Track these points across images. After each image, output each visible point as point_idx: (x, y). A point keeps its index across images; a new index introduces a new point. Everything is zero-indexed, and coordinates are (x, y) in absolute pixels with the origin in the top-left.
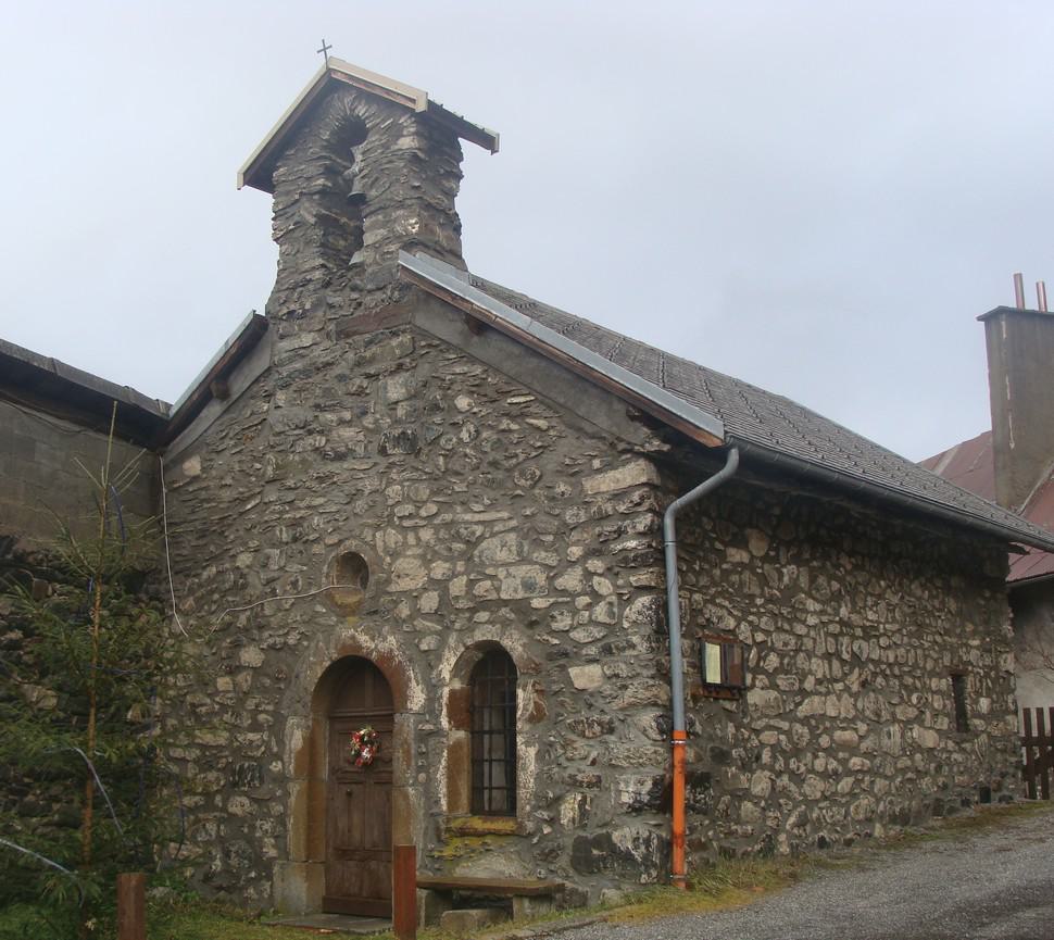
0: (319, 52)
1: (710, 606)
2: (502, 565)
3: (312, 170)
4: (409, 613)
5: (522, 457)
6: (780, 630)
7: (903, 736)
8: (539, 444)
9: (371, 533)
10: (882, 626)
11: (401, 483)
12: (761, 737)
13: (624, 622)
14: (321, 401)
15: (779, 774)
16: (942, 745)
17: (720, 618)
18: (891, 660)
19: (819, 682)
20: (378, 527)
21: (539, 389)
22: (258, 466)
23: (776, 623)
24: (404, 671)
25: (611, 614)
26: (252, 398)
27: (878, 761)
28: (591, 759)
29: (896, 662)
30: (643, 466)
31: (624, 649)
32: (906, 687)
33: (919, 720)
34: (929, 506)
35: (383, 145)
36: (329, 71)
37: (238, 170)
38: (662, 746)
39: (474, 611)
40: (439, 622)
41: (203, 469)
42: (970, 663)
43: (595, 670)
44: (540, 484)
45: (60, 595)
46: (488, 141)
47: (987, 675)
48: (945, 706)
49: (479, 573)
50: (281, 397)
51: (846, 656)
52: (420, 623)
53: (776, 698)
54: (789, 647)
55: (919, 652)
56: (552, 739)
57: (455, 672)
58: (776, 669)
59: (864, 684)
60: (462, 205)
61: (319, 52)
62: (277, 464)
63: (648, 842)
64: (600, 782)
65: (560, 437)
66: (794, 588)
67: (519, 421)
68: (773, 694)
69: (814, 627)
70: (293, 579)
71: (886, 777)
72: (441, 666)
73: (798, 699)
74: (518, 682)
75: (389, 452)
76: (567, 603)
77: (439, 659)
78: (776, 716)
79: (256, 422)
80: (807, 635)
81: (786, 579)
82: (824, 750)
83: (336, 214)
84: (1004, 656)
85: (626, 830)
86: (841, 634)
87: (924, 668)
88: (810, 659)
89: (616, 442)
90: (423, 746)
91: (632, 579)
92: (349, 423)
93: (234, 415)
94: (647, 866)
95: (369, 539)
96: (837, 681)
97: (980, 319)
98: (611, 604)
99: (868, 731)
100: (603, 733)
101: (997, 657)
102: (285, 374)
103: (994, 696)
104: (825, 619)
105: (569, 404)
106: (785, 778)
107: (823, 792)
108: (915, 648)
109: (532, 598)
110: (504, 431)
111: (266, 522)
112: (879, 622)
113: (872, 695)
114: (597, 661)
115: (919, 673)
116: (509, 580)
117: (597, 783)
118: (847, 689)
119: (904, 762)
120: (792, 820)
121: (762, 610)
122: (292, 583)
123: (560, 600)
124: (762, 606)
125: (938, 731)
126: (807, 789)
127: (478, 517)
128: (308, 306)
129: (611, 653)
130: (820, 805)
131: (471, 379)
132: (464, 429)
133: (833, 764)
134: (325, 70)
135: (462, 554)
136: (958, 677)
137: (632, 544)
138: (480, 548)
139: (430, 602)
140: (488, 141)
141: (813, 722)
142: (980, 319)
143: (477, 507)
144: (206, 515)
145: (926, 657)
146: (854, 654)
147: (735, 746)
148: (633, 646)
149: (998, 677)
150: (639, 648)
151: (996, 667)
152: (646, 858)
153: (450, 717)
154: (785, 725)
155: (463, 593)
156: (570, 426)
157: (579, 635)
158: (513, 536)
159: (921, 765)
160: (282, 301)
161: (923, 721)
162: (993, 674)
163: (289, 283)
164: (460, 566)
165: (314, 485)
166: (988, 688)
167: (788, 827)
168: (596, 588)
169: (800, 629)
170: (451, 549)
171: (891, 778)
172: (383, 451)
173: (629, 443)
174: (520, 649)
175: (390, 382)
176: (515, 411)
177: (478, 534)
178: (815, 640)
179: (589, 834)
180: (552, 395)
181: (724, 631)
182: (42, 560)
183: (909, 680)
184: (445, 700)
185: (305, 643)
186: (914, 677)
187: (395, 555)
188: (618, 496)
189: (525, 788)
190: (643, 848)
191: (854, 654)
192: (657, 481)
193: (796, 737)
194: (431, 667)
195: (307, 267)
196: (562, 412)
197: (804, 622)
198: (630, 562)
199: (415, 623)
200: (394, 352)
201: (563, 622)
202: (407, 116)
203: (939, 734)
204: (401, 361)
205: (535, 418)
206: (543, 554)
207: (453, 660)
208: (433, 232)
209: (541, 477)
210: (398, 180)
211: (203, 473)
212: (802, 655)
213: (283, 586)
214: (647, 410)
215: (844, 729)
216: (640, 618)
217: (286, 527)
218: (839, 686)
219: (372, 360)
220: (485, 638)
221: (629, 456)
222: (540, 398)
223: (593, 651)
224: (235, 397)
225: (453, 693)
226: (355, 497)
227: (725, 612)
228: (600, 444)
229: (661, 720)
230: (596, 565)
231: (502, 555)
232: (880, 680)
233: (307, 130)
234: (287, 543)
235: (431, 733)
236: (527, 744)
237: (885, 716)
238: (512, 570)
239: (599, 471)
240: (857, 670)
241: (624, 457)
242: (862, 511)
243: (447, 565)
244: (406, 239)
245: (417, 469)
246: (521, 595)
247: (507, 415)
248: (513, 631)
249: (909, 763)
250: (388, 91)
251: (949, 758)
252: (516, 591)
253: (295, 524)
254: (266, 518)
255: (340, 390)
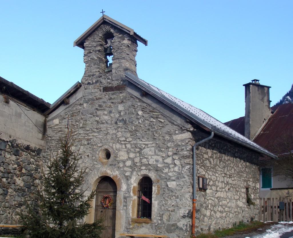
0: (101, 12)
1: (200, 169)
2: (150, 155)
3: (95, 44)
4: (122, 166)
5: (156, 128)
6: (213, 175)
7: (236, 203)
8: (161, 126)
9: (112, 144)
10: (233, 175)
11: (121, 132)
12: (209, 202)
13: (183, 172)
14: (98, 108)
15: (212, 211)
16: (244, 206)
17: (202, 172)
18: (234, 184)
19: (220, 188)
20: (114, 143)
21: (162, 112)
22: (77, 123)
23: (212, 173)
24: (121, 180)
25: (179, 170)
26: (76, 104)
27: (230, 209)
28: (172, 205)
29: (235, 184)
30: (189, 135)
31: (182, 178)
32: (237, 191)
33: (239, 199)
34: (251, 147)
35: (119, 42)
36: (103, 18)
37: (74, 40)
38: (191, 202)
39: (141, 166)
40: (131, 168)
41: (60, 123)
42: (250, 185)
43: (174, 183)
44: (161, 136)
45: (25, 155)
46: (145, 42)
47: (253, 189)
48: (244, 196)
49: (143, 157)
50: (85, 105)
51: (226, 182)
52: (125, 169)
53: (212, 192)
54: (215, 179)
55: (240, 182)
56: (162, 199)
57: (135, 182)
58: (212, 185)
59: (229, 189)
60: (137, 58)
61: (101, 12)
62: (83, 123)
63: (187, 225)
64: (174, 210)
65: (167, 124)
66: (216, 165)
67: (156, 119)
68: (211, 191)
69: (220, 174)
70: (87, 154)
71: (232, 213)
72: (131, 180)
73: (216, 192)
74: (153, 185)
75: (118, 123)
76: (167, 166)
77: (131, 178)
78: (212, 196)
79: (77, 111)
80: (218, 177)
81: (215, 162)
82: (220, 205)
83: (102, 57)
84: (257, 184)
85: (181, 222)
86: (225, 176)
87: (241, 186)
88: (218, 183)
89: (182, 127)
90: (125, 200)
91: (185, 161)
92: (106, 115)
93: (70, 109)
94: (186, 231)
95: (111, 145)
96: (223, 188)
97: (244, 85)
98: (179, 167)
99: (229, 201)
100: (176, 198)
101: (256, 184)
102: (87, 100)
103: (255, 194)
104: (222, 172)
105: (170, 117)
106: (213, 212)
107: (220, 216)
108: (239, 180)
109: (158, 164)
110: (151, 121)
111: (80, 138)
112: (232, 174)
113: (230, 192)
114: (174, 180)
115: (239, 187)
116: (152, 159)
117: (173, 211)
118: (225, 190)
119: (236, 210)
120: (214, 222)
121: (210, 170)
122: (87, 155)
123: (165, 165)
124: (210, 169)
125: (243, 202)
126: (217, 215)
127: (143, 143)
128: (94, 82)
129: (179, 179)
130: (219, 219)
131: (143, 107)
132: (140, 120)
133: (222, 209)
134: (102, 18)
135: (139, 152)
136: (247, 189)
137: (186, 153)
138: (143, 150)
139: (129, 163)
140: (145, 42)
141: (219, 198)
142: (244, 85)
143: (143, 140)
144: (60, 135)
145: (241, 183)
146: (227, 182)
147: (204, 203)
148: (185, 178)
149: (256, 189)
150: (186, 178)
151: (255, 187)
152: (186, 229)
153: (133, 193)
154: (213, 199)
155: (138, 162)
156: (170, 122)
157: (170, 174)
158: (153, 148)
159: (239, 211)
160: (86, 79)
161: (240, 200)
162: (254, 188)
163: (87, 75)
164: (138, 155)
165: (95, 130)
166: (253, 192)
167: (213, 224)
168: (175, 163)
169: (217, 175)
170: (135, 150)
171: (233, 214)
172: (116, 123)
173: (186, 128)
174: (154, 177)
175: (119, 105)
176: (155, 116)
177: (143, 147)
178: (220, 178)
179: (171, 223)
180: (165, 114)
181: (203, 175)
182: (22, 146)
183: (237, 189)
184: (132, 188)
185: (91, 172)
186: (239, 188)
187: (119, 150)
188: (182, 141)
189: (154, 211)
190: (185, 227)
191: (227, 182)
192: (192, 138)
193: (215, 202)
194: (128, 180)
195: (94, 71)
196: (168, 118)
197: (218, 173)
198: (184, 157)
199: (124, 168)
200: (121, 98)
201: (166, 170)
202: (126, 35)
203: (243, 203)
204: (123, 100)
205: (160, 119)
206: (161, 153)
207: (135, 178)
208: (131, 66)
209: (161, 134)
210: (123, 52)
211: (60, 123)
212: (217, 181)
213: (84, 156)
214: (191, 120)
215: (225, 200)
216: (187, 171)
217: (86, 140)
218: (224, 190)
219: (114, 99)
220: (144, 173)
221: (186, 131)
222: (162, 114)
223: (174, 178)
224: (71, 104)
225: (134, 187)
226: (107, 134)
227: (203, 170)
228: (178, 127)
229: (191, 196)
230: (176, 157)
231: (150, 153)
232: (232, 188)
233: (95, 33)
234: (86, 145)
235: (128, 197)
236: (155, 200)
237: (233, 198)
238: (153, 157)
239: (177, 134)
240: (228, 186)
241: (184, 131)
242: (231, 145)
243: (134, 154)
244: (125, 68)
245: (126, 129)
246: (155, 163)
247: (152, 117)
248: (152, 172)
249: (237, 210)
250: (122, 27)
251: (245, 209)
252: (153, 162)
253: (88, 140)
254: (80, 138)
255: (104, 105)
